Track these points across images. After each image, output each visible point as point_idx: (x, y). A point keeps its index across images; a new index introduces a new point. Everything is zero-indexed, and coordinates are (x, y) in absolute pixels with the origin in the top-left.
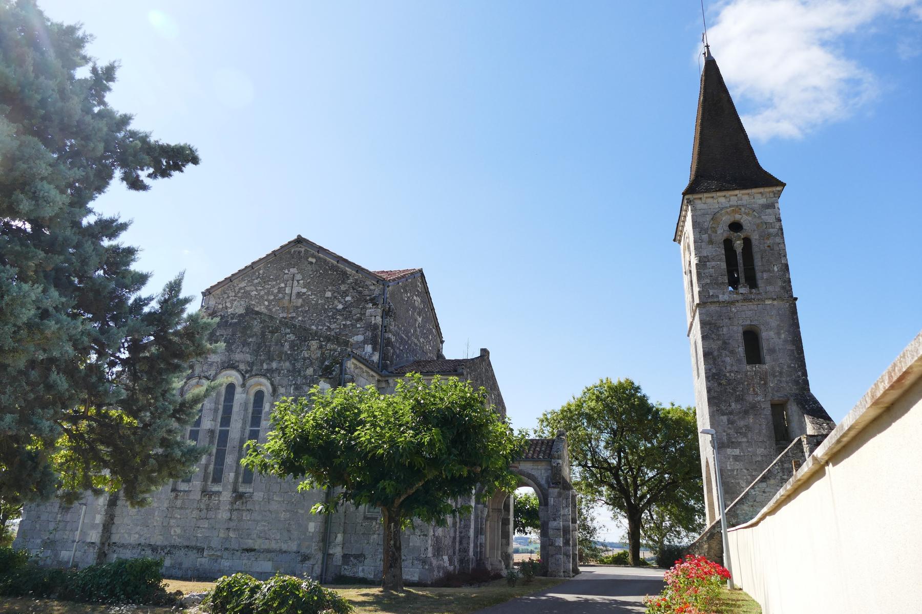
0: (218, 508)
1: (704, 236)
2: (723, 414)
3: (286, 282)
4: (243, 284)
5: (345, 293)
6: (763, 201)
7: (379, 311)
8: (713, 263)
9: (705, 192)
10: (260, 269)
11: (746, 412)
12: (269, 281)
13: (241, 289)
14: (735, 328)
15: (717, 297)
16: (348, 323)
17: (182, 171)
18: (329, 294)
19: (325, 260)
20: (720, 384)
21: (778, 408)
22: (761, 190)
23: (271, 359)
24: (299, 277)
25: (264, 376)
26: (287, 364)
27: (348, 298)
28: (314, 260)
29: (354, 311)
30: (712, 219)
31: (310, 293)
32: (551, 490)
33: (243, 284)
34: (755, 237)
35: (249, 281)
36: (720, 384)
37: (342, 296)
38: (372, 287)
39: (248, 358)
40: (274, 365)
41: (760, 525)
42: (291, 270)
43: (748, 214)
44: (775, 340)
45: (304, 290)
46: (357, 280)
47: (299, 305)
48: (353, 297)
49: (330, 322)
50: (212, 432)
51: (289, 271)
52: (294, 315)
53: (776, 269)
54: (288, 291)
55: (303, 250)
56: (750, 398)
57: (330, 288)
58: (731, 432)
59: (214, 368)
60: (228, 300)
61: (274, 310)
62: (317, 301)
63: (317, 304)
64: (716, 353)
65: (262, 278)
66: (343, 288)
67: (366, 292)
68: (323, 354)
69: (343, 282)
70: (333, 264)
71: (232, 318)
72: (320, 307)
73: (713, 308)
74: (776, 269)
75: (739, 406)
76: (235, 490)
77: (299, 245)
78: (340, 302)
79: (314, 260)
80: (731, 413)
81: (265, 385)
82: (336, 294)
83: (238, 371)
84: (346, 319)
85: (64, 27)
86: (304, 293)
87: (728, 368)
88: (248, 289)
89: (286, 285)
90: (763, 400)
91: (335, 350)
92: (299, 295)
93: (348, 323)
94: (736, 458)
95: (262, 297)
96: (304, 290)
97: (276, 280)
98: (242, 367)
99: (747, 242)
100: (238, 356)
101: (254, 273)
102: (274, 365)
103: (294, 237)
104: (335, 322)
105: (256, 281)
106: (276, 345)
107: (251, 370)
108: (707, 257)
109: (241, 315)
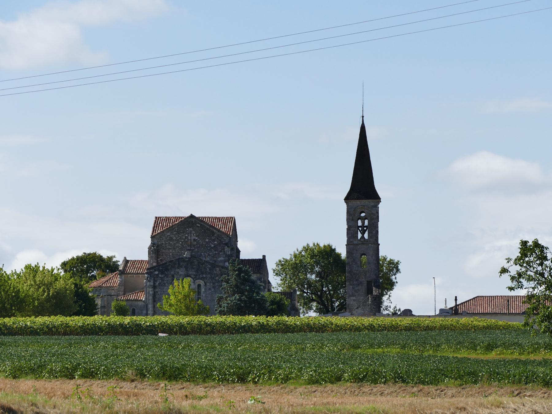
1: (350, 217)
2: (351, 285)
3: (188, 234)
4: (169, 234)
5: (214, 240)
6: (373, 204)
7: (230, 249)
8: (353, 229)
9: (352, 200)
11: (359, 285)
13: (168, 236)
14: (358, 254)
15: (353, 242)
16: (217, 252)
17: (308, 245)
18: (207, 240)
19: (204, 226)
20: (351, 275)
21: (369, 283)
22: (373, 200)
23: (203, 274)
24: (193, 232)
25: (201, 279)
26: (209, 275)
27: (216, 242)
28: (199, 225)
30: (354, 211)
32: (292, 312)
33: (169, 234)
35: (171, 233)
36: (351, 275)
39: (194, 273)
40: (204, 276)
41: (454, 301)
43: (367, 209)
45: (197, 238)
46: (218, 235)
47: (195, 244)
48: (217, 242)
49: (209, 252)
51: (189, 229)
52: (194, 248)
53: (374, 232)
54: (189, 238)
55: (194, 220)
56: (360, 280)
57: (207, 238)
58: (353, 291)
60: (163, 240)
62: (203, 243)
63: (202, 244)
64: (351, 263)
65: (177, 232)
66: (213, 238)
67: (223, 240)
68: (221, 272)
69: (213, 236)
71: (186, 259)
72: (204, 245)
73: (351, 246)
74: (374, 232)
75: (356, 283)
77: (192, 218)
78: (212, 244)
79: (199, 225)
80: (354, 285)
81: (202, 282)
83: (191, 278)
84: (215, 251)
86: (197, 240)
87: (354, 269)
88: (171, 236)
89: (188, 235)
90: (364, 280)
91: (225, 271)
92: (194, 240)
93: (217, 252)
94: (354, 300)
96: (197, 238)
97: (183, 233)
98: (192, 276)
100: (190, 273)
101: (173, 229)
102: (204, 276)
104: (211, 252)
105: (174, 233)
106: (204, 269)
107: (196, 278)
109: (189, 258)
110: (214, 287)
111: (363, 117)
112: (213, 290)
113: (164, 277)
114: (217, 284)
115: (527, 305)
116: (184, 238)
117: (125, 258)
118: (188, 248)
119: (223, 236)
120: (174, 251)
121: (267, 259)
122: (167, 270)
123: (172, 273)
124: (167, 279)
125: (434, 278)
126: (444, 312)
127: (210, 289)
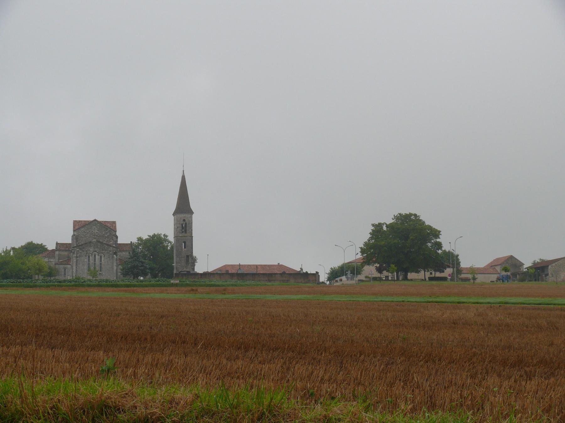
5: (107, 233)
18: (104, 233)
24: (96, 228)
25: (102, 253)
34: (187, 223)
50: (93, 263)
54: (94, 231)
66: (107, 232)
69: (107, 231)
85: (151, 236)
94: (179, 265)
99: (186, 224)
100: (96, 250)
103: (94, 219)
111: (183, 171)
115: (97, 257)
117: (57, 242)
119: (112, 231)
121: (149, 235)
125: (450, 243)
126: (342, 285)
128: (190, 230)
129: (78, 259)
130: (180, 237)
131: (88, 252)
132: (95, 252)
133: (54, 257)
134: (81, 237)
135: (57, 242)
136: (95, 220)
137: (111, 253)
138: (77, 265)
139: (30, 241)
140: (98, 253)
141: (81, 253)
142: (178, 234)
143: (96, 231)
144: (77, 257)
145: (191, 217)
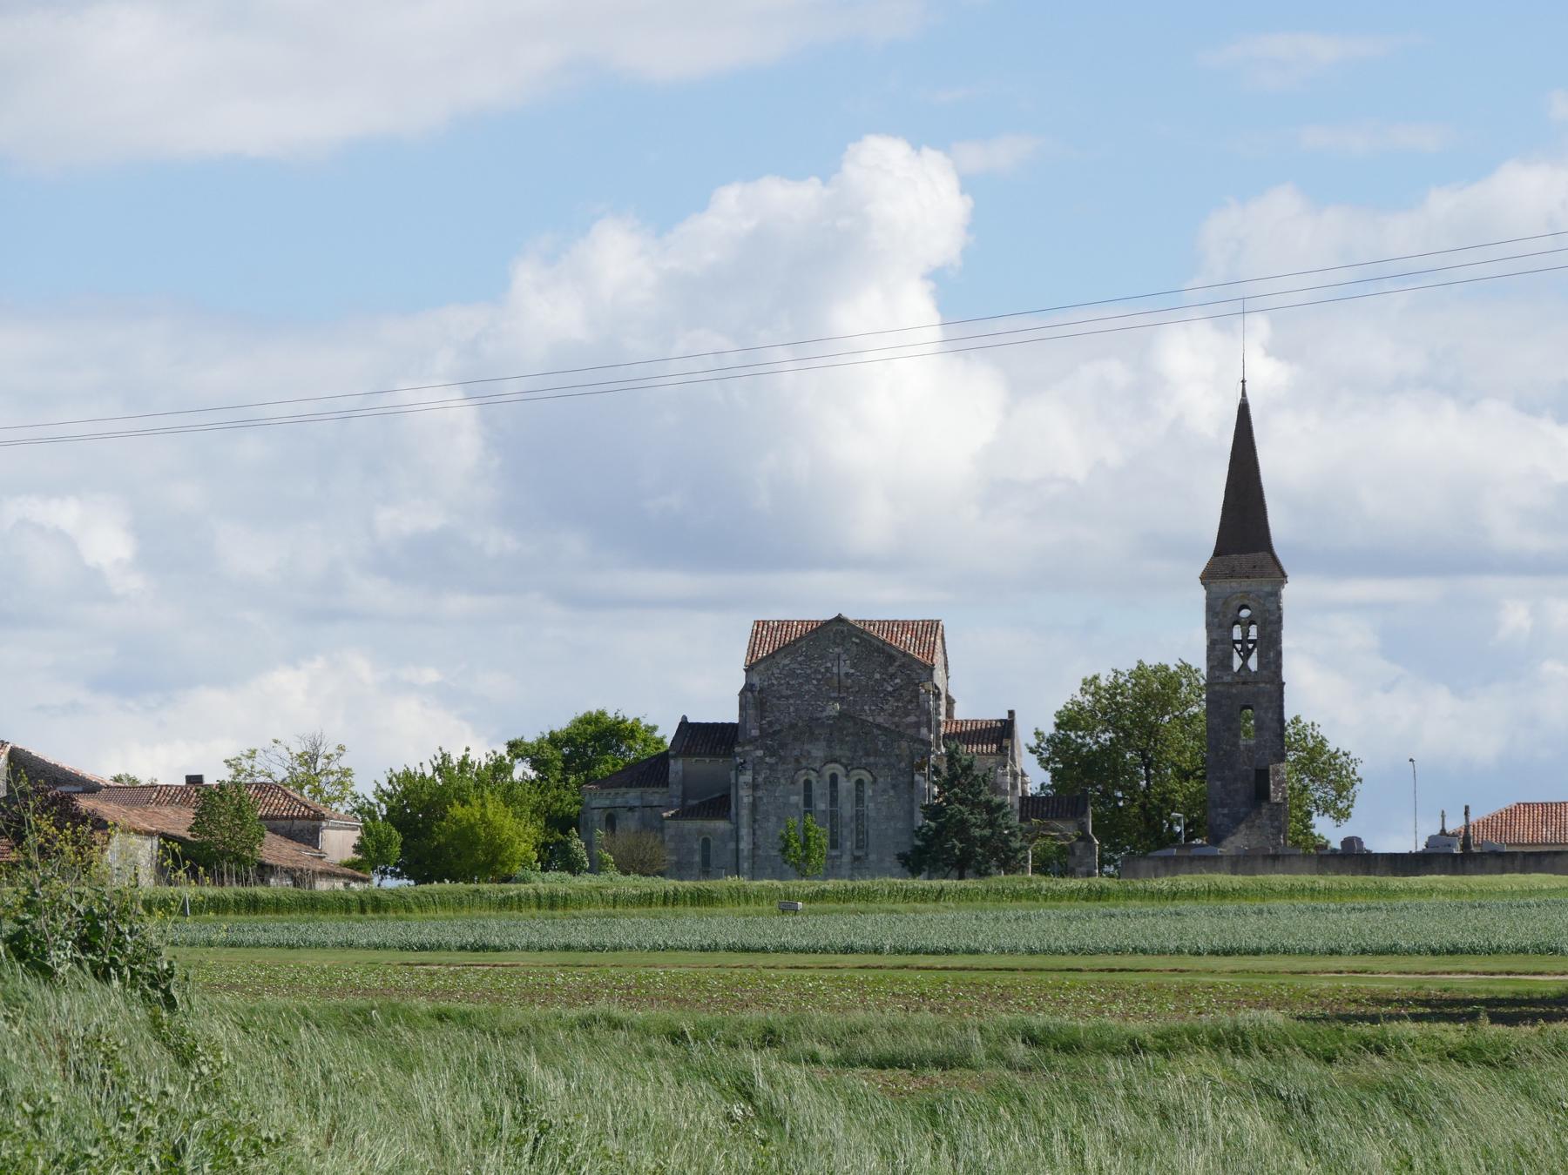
0: (839, 867)
4: (787, 661)
5: (893, 676)
10: (802, 646)
12: (814, 659)
13: (785, 666)
15: (1222, 678)
18: (877, 676)
24: (844, 657)
25: (865, 768)
27: (898, 681)
28: (857, 641)
29: (905, 693)
31: (858, 674)
33: (787, 661)
37: (891, 678)
38: (920, 671)
42: (836, 649)
44: (911, 1107)
45: (852, 671)
48: (902, 681)
49: (882, 703)
52: (845, 695)
54: (835, 670)
59: (818, 761)
61: (824, 689)
66: (891, 670)
68: (911, 752)
70: (878, 646)
76: (852, 854)
77: (841, 624)
79: (857, 641)
81: (837, 769)
82: (884, 676)
83: (841, 764)
84: (898, 701)
91: (921, 749)
93: (900, 704)
94: (1224, 815)
95: (809, 675)
96: (852, 671)
100: (838, 753)
108: (1216, 640)
110: (894, 787)
112: (892, 793)
113: (777, 763)
114: (901, 778)
116: (823, 670)
117: (684, 718)
118: (833, 695)
120: (799, 702)
122: (783, 746)
123: (796, 752)
124: (785, 766)
127: (885, 791)
128: (1272, 654)
129: (760, 794)
130: (1223, 683)
131: (804, 763)
132: (832, 762)
133: (666, 784)
134: (782, 696)
135: (684, 718)
136: (839, 620)
137: (903, 765)
138: (755, 821)
139: (593, 707)
140: (846, 767)
141: (771, 767)
142: (1217, 673)
143: (846, 668)
144: (755, 786)
145: (1276, 595)
